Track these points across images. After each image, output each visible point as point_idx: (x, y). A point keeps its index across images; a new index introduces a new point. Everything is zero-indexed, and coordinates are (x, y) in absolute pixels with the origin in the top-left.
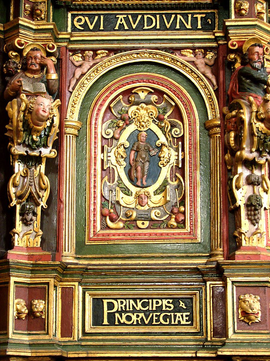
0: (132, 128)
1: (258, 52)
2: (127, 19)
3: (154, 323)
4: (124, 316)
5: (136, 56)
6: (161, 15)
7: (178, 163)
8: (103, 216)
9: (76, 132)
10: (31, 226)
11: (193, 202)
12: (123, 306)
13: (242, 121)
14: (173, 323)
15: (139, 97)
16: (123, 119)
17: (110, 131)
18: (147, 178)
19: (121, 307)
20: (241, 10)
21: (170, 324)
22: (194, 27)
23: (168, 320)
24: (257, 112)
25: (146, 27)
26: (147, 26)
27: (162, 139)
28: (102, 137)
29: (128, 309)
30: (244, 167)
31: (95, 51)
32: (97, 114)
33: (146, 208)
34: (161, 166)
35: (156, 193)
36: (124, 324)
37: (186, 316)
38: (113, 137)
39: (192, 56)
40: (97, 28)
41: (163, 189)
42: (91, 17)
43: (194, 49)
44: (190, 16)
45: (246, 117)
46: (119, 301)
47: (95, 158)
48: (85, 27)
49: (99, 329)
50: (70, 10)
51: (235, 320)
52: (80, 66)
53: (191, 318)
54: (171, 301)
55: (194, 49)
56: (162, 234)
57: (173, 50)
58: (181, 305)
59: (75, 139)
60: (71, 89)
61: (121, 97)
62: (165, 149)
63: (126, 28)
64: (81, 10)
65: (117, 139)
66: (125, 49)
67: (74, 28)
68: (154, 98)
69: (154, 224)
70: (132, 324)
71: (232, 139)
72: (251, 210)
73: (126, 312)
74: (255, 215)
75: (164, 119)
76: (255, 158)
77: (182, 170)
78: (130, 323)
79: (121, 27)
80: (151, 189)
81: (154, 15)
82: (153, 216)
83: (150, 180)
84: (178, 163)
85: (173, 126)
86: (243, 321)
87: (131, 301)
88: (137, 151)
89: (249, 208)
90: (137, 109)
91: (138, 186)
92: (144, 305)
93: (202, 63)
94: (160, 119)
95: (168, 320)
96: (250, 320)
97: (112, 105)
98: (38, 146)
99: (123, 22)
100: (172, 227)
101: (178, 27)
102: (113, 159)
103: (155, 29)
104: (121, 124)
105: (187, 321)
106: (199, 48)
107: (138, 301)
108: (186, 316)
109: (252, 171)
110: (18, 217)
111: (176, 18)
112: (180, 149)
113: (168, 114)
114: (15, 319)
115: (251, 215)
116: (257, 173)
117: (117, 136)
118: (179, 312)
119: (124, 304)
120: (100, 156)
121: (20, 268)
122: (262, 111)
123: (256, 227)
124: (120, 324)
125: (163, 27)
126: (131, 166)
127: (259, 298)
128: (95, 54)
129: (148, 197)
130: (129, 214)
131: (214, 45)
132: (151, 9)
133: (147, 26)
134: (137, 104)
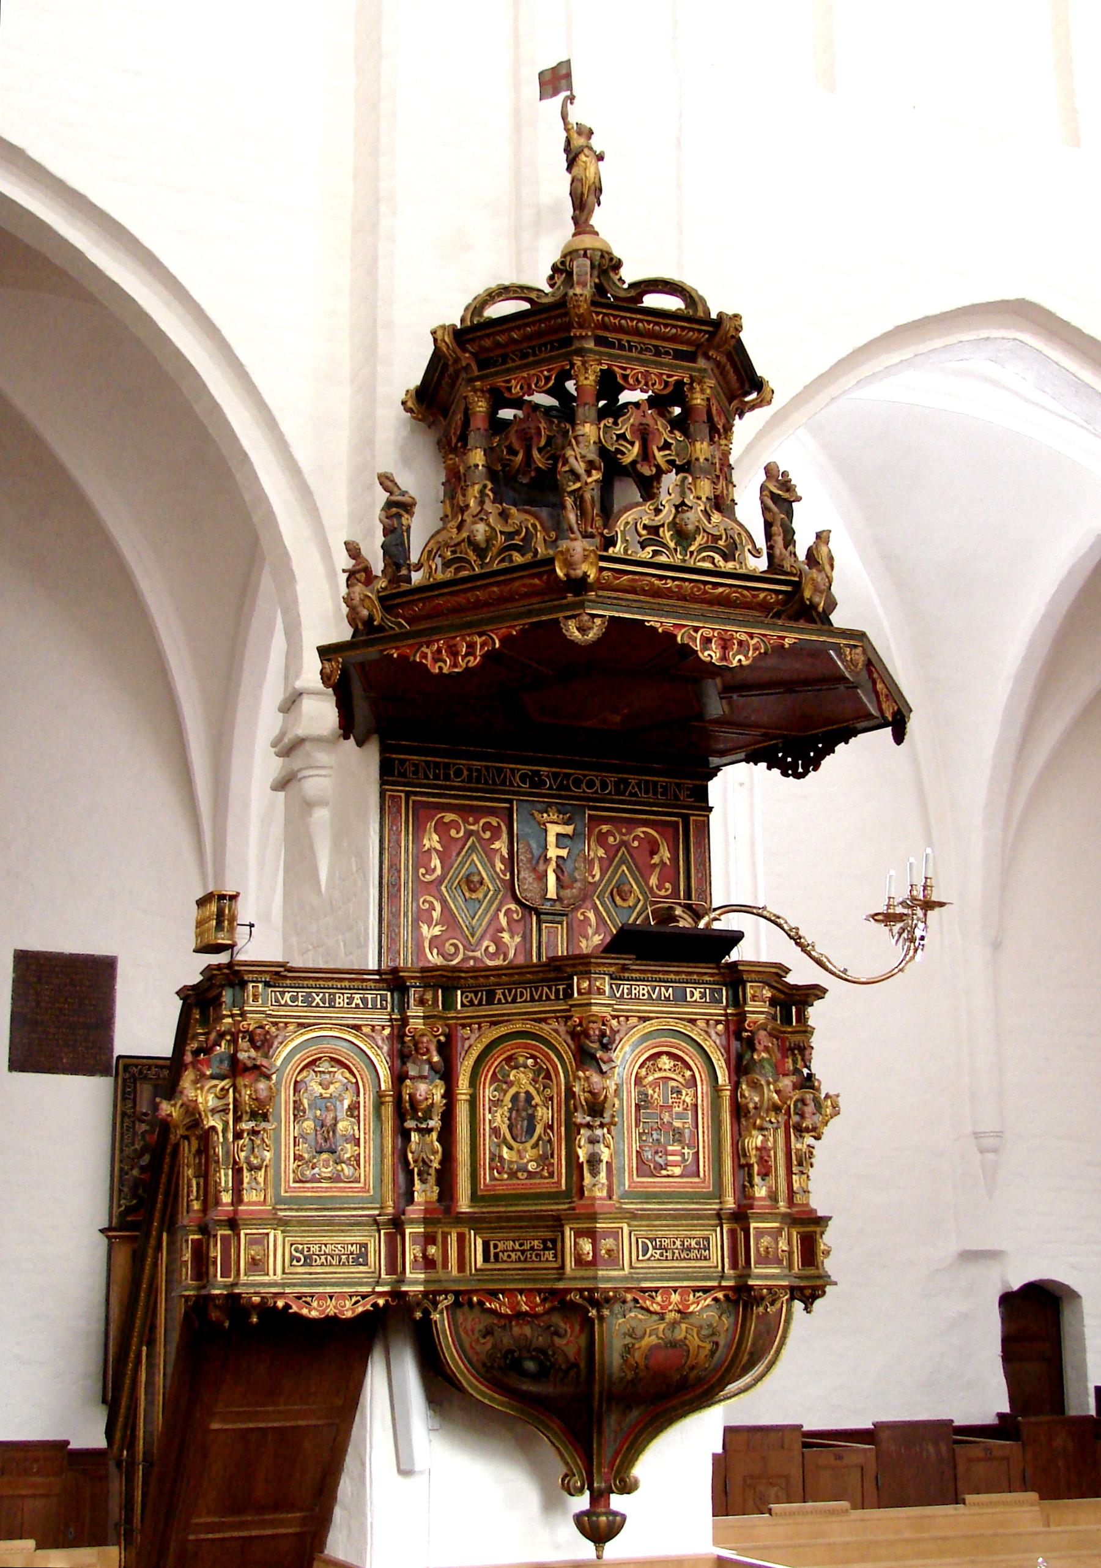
0: (513, 1091)
2: (504, 994)
4: (506, 1254)
8: (491, 1169)
16: (506, 1083)
17: (496, 1093)
21: (540, 1261)
22: (557, 998)
25: (519, 1000)
35: (532, 1148)
38: (498, 1100)
40: (480, 1004)
43: (557, 1018)
49: (488, 1266)
50: (459, 989)
52: (468, 1038)
53: (555, 1256)
55: (557, 1018)
62: (538, 1108)
63: (503, 1001)
65: (502, 1101)
67: (463, 1005)
68: (530, 1062)
69: (531, 1175)
70: (512, 1262)
73: (507, 1251)
77: (551, 1127)
80: (529, 1145)
81: (525, 989)
82: (530, 1168)
88: (518, 1111)
92: (521, 1245)
94: (536, 1082)
100: (545, 1178)
101: (544, 998)
102: (499, 1119)
104: (505, 1086)
106: (562, 1017)
110: (416, 1177)
111: (543, 990)
116: (599, 1132)
120: (488, 1116)
121: (412, 1222)
125: (533, 1000)
128: (480, 1028)
130: (512, 1166)
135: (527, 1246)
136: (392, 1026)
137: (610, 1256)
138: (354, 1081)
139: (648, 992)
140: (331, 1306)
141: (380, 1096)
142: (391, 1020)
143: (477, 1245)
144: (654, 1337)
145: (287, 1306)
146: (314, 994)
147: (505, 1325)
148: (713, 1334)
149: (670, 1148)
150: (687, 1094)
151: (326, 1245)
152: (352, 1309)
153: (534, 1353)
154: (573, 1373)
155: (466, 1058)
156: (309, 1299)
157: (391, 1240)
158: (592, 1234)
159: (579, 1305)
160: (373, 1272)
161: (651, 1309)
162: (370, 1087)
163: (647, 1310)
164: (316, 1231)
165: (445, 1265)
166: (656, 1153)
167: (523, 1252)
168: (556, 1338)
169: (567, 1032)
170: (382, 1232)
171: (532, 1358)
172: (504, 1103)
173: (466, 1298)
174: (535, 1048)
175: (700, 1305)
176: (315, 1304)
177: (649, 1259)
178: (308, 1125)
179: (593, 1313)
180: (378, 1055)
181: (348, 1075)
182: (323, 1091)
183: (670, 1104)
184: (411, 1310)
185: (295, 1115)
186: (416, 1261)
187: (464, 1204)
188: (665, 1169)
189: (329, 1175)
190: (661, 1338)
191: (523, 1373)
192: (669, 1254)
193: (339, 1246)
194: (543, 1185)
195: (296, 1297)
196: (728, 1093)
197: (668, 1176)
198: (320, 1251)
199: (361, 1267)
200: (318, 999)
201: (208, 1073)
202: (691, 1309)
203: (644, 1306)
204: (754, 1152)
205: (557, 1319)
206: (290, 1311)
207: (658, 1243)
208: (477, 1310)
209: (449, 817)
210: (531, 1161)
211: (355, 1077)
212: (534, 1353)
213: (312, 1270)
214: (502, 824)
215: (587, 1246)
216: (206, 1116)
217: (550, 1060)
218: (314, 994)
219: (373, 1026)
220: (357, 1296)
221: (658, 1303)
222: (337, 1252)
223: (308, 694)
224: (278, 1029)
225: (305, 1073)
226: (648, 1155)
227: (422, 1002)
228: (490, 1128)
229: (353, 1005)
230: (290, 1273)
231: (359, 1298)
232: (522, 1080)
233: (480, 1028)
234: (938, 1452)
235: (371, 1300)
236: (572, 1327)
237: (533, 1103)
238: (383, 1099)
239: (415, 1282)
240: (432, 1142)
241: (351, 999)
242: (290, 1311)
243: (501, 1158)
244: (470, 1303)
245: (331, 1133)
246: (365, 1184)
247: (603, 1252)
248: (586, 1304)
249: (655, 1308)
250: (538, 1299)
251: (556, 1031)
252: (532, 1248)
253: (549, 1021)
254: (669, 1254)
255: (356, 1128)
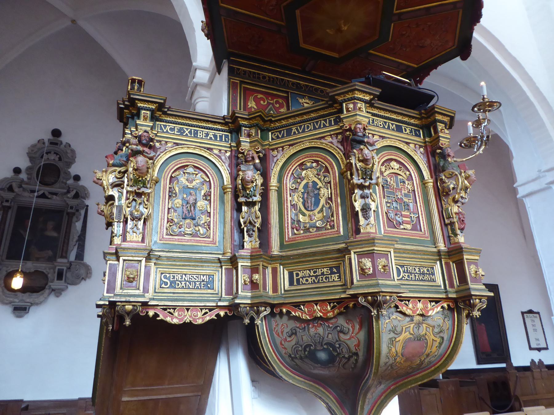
1: (359, 127)
2: (297, 129)
3: (320, 282)
5: (302, 145)
6: (313, 123)
7: (328, 195)
8: (292, 228)
9: (277, 189)
10: (253, 237)
11: (338, 214)
12: (303, 274)
13: (351, 164)
14: (330, 281)
15: (307, 166)
16: (300, 178)
17: (293, 185)
18: (314, 206)
19: (303, 275)
20: (348, 108)
21: (329, 281)
23: (327, 279)
24: (358, 157)
25: (306, 130)
26: (307, 129)
27: (320, 184)
28: (290, 189)
29: (306, 276)
30: (359, 190)
31: (282, 147)
32: (287, 178)
33: (314, 221)
34: (320, 198)
35: (319, 213)
36: (305, 284)
37: (337, 276)
39: (331, 139)
40: (283, 136)
41: (321, 210)
42: (280, 132)
43: (331, 135)
44: (328, 120)
45: (353, 161)
46: (301, 272)
47: (287, 200)
48: (278, 137)
49: (293, 288)
50: (270, 131)
51: (358, 274)
53: (340, 277)
54: (328, 269)
55: (331, 135)
56: (322, 234)
57: (320, 138)
58: (334, 271)
59: (277, 192)
60: (272, 168)
61: (298, 167)
62: (321, 189)
63: (297, 133)
64: (274, 129)
65: (297, 189)
66: (297, 143)
67: (272, 139)
68: (314, 164)
70: (309, 284)
71: (349, 175)
72: (364, 212)
73: (305, 277)
74: (366, 214)
75: (320, 174)
76: (362, 183)
77: (330, 199)
78: (308, 283)
79: (295, 133)
80: (316, 212)
81: (310, 124)
82: (318, 225)
83: (315, 207)
84: (328, 195)
85: (325, 177)
86: (362, 274)
87: (308, 271)
88: (308, 193)
89: (363, 211)
90: (307, 172)
91: (309, 211)
92: (315, 272)
93: (336, 141)
94: (318, 175)
95: (327, 279)
96: (366, 273)
97: (294, 172)
98: (251, 197)
99: (295, 130)
100: (328, 229)
102: (296, 199)
103: (311, 130)
104: (299, 181)
105: (338, 279)
106: (334, 134)
107: (311, 270)
108: (337, 276)
109: (363, 191)
112: (329, 188)
113: (322, 171)
114: (243, 285)
115: (364, 215)
116: (367, 191)
117: (297, 187)
118: (333, 274)
119: (304, 273)
120: (289, 198)
121: (243, 258)
122: (360, 156)
123: (368, 221)
124: (303, 284)
125: (315, 128)
126: (305, 201)
127: (370, 260)
128: (283, 149)
129: (315, 215)
131: (341, 131)
132: (308, 121)
133: (307, 129)
134: (306, 169)
135: (319, 272)
136: (231, 151)
137: (385, 270)
138: (208, 180)
139: (383, 124)
140: (188, 316)
141: (223, 189)
142: (231, 147)
143: (284, 275)
144: (408, 333)
145: (156, 315)
146: (185, 129)
147: (305, 327)
148: (441, 332)
149: (403, 213)
150: (408, 184)
151: (185, 275)
152: (202, 318)
153: (325, 347)
154: (353, 360)
155: (275, 167)
156: (172, 311)
157: (229, 272)
158: (370, 254)
159: (363, 306)
160: (217, 294)
161: (407, 313)
162: (217, 183)
163: (404, 314)
164: (180, 265)
165: (265, 288)
166: (396, 215)
167: (316, 277)
168: (341, 335)
169: (338, 142)
170: (223, 267)
171: (324, 350)
172: (299, 190)
173: (279, 310)
174: (317, 156)
175: (435, 311)
176: (176, 314)
177: (401, 279)
178: (178, 202)
179: (374, 312)
180: (223, 166)
181: (204, 177)
182: (188, 184)
183: (400, 188)
184: (241, 318)
185: (170, 196)
186: (245, 284)
187: (275, 250)
188: (402, 225)
189: (190, 233)
190: (412, 334)
191: (316, 360)
192: (413, 276)
193: (195, 276)
194: (329, 233)
195: (163, 309)
196: (432, 184)
197: (404, 229)
198: (182, 278)
199: (209, 290)
200: (187, 132)
201: (111, 162)
202: (429, 314)
203: (402, 310)
204: (454, 216)
205: (341, 321)
206: (158, 319)
207: (406, 269)
208: (285, 318)
209: (260, 96)
210: (318, 221)
211: (208, 177)
212: (325, 347)
213: (177, 291)
214: (284, 102)
215: (368, 263)
216: (108, 188)
217: (327, 161)
218: (185, 129)
219: (220, 150)
220: (206, 309)
221: (410, 309)
222: (193, 280)
223: (199, 69)
224: (161, 144)
225: (177, 173)
226: (392, 215)
227: (249, 136)
228: (291, 205)
229: (208, 138)
230: (160, 292)
231: (207, 310)
232: (310, 175)
233: (283, 150)
234: (415, 392)
235: (215, 312)
236: (353, 329)
237: (318, 187)
238: (225, 191)
239: (245, 298)
240: (255, 212)
241: (207, 135)
242: (158, 319)
243: (299, 221)
244: (281, 314)
245: (192, 208)
246: (213, 239)
247: (380, 267)
248: (369, 306)
249: (409, 312)
250: (329, 307)
251: (331, 143)
252: (323, 274)
253: (326, 138)
254: (413, 276)
255: (208, 207)
